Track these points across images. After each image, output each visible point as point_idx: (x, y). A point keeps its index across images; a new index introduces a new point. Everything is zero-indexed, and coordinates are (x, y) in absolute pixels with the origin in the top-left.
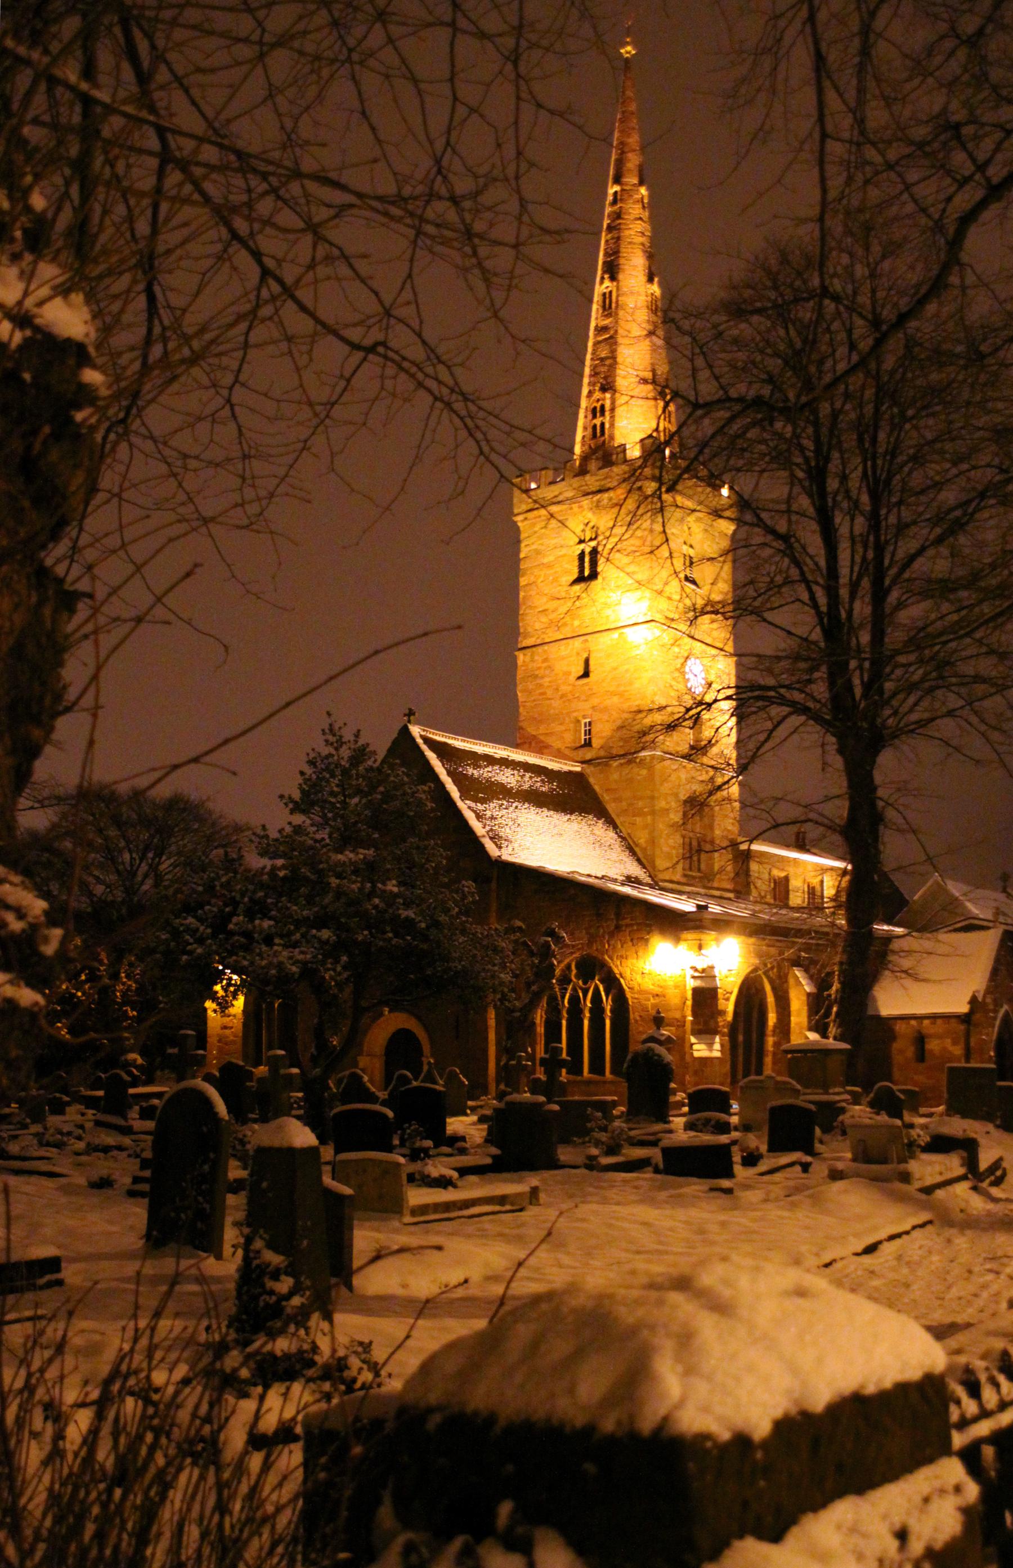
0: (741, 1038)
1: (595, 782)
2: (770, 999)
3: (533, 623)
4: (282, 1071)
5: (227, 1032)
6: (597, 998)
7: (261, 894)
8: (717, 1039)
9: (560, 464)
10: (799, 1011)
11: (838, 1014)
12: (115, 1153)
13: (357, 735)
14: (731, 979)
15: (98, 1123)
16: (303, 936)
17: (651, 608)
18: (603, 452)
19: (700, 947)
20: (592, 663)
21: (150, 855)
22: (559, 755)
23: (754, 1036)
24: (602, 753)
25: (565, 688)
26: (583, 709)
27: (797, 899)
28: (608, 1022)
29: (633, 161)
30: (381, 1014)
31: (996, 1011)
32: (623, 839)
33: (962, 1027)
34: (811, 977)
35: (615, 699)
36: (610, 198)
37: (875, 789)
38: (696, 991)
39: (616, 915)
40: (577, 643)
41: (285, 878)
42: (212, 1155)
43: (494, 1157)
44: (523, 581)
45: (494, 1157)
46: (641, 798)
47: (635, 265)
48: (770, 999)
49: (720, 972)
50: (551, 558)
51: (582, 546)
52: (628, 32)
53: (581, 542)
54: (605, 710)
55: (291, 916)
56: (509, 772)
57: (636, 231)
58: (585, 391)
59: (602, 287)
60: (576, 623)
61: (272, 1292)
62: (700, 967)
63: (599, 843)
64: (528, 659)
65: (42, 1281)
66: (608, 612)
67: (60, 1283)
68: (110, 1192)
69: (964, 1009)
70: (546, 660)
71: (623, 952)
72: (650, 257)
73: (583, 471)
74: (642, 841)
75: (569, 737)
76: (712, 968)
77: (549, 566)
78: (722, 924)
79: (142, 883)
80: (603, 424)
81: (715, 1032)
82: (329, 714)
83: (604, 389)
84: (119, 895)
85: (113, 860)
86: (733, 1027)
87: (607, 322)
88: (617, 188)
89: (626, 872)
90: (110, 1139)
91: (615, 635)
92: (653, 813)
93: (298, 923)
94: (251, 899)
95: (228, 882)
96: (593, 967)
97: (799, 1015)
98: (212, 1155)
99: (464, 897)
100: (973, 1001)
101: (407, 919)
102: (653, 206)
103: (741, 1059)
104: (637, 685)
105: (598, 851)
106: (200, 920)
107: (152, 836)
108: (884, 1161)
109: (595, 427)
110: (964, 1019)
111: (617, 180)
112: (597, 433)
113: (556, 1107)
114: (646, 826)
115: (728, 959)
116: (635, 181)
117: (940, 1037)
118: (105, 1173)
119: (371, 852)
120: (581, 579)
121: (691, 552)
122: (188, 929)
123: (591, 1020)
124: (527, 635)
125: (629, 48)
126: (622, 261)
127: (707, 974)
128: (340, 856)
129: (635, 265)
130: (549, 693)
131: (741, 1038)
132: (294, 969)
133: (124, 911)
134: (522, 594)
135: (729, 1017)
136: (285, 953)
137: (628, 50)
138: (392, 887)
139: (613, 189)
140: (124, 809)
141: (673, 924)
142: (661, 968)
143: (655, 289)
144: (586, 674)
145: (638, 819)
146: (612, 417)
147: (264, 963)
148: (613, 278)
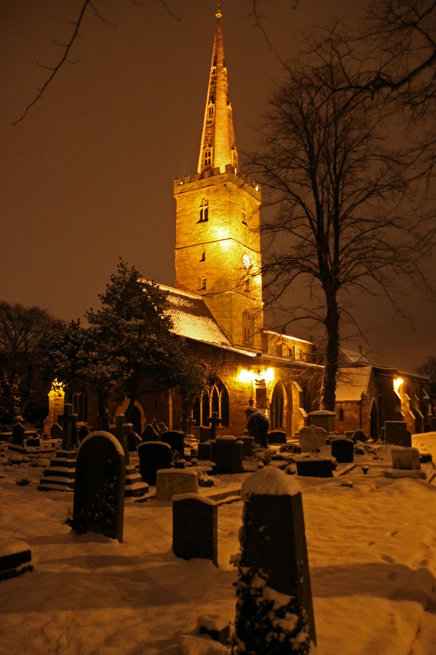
0: (274, 410)
1: (208, 304)
2: (285, 394)
3: (182, 239)
4: (124, 425)
5: (57, 407)
6: (215, 393)
7: (90, 340)
8: (267, 411)
9: (192, 174)
10: (296, 399)
11: (323, 400)
12: (23, 464)
13: (133, 268)
14: (271, 385)
15: (10, 448)
16: (112, 359)
17: (230, 233)
18: (210, 170)
19: (259, 372)
20: (206, 255)
21: (23, 332)
22: (193, 292)
23: (279, 410)
24: (210, 292)
25: (194, 265)
26: (202, 274)
27: (285, 353)
28: (220, 403)
29: (221, 57)
30: (124, 400)
31: (370, 400)
32: (220, 327)
33: (358, 406)
34: (300, 385)
35: (216, 270)
36: (212, 71)
37: (337, 304)
38: (257, 390)
39: (224, 358)
40: (200, 247)
41: (100, 334)
42: (115, 478)
43: (213, 467)
44: (178, 221)
45: (213, 467)
46: (226, 311)
47: (222, 97)
48: (285, 394)
49: (266, 382)
50: (189, 212)
51: (201, 208)
52: (219, 8)
53: (201, 206)
54: (211, 274)
55: (106, 350)
56: (174, 298)
57: (223, 84)
58: (202, 146)
59: (209, 106)
60: (199, 239)
61: (279, 630)
62: (259, 380)
63: (210, 329)
64: (180, 253)
65: (19, 569)
66: (213, 235)
67: (30, 568)
68: (27, 488)
69: (359, 399)
70: (187, 254)
71: (226, 374)
72: (228, 95)
73: (202, 177)
74: (227, 329)
75: (196, 285)
76: (264, 380)
77: (189, 215)
78: (267, 363)
79: (20, 344)
80: (210, 160)
81: (266, 408)
82: (120, 258)
83: (210, 146)
84: (10, 349)
85: (8, 334)
86: (271, 405)
87: (211, 119)
88: (215, 68)
89: (221, 341)
90: (20, 457)
91: (215, 244)
92: (231, 317)
93: (110, 354)
94: (86, 343)
95: (75, 334)
96: (214, 380)
97: (296, 401)
98: (115, 478)
99: (181, 343)
100: (363, 395)
101: (160, 352)
102: (229, 75)
103: (274, 419)
104: (224, 264)
105: (210, 332)
106: (62, 352)
107: (24, 325)
108: (410, 469)
109: (206, 160)
110: (359, 403)
111: (215, 64)
112: (207, 163)
113: (242, 442)
114: (228, 322)
115: (270, 376)
116: (222, 65)
117: (350, 410)
118: (25, 477)
119: (143, 321)
120: (201, 221)
121: (244, 212)
122: (57, 356)
123: (213, 402)
124: (179, 243)
125: (219, 14)
126: (217, 96)
127: (262, 383)
128: (129, 322)
129: (222, 97)
130: (189, 267)
131: (274, 410)
132: (109, 375)
133: (12, 355)
134: (177, 227)
135: (270, 401)
136: (104, 367)
137: (219, 15)
138: (153, 337)
139: (213, 68)
140: (13, 313)
141: (248, 362)
142: (244, 379)
143: (230, 107)
144: (203, 260)
145: (225, 319)
146: (213, 157)
147: (95, 372)
148: (213, 102)
